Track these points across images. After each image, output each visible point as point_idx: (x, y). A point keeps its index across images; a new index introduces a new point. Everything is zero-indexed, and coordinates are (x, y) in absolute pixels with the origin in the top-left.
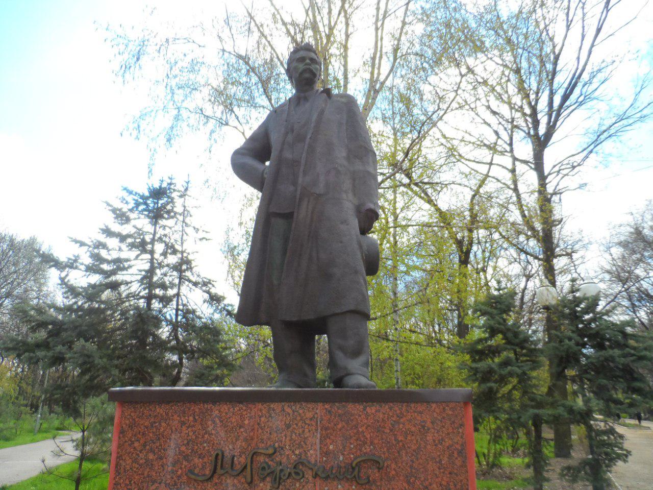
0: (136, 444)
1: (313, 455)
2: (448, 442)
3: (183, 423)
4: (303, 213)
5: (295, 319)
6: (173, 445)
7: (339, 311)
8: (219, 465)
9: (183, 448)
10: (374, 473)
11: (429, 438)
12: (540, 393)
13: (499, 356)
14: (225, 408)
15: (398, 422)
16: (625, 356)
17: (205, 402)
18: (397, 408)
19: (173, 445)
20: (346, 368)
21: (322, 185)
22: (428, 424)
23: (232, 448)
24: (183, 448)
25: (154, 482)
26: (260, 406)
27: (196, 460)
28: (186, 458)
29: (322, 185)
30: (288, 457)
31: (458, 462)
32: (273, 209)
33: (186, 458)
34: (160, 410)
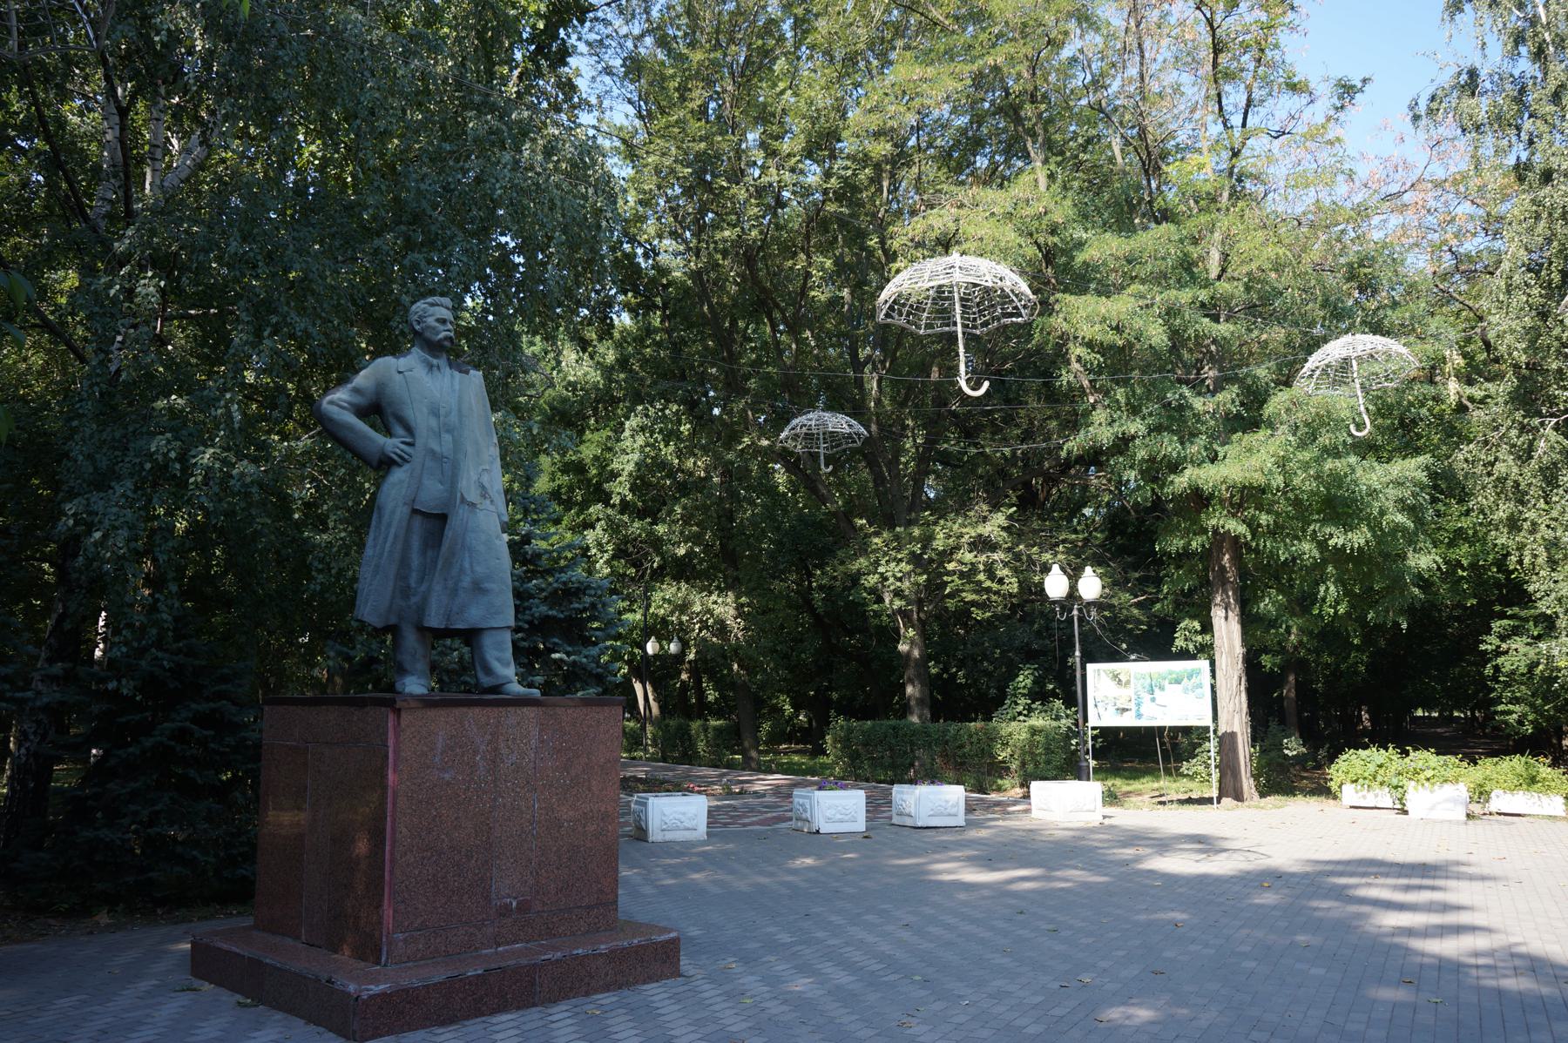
4: (454, 523)
14: (477, 710)
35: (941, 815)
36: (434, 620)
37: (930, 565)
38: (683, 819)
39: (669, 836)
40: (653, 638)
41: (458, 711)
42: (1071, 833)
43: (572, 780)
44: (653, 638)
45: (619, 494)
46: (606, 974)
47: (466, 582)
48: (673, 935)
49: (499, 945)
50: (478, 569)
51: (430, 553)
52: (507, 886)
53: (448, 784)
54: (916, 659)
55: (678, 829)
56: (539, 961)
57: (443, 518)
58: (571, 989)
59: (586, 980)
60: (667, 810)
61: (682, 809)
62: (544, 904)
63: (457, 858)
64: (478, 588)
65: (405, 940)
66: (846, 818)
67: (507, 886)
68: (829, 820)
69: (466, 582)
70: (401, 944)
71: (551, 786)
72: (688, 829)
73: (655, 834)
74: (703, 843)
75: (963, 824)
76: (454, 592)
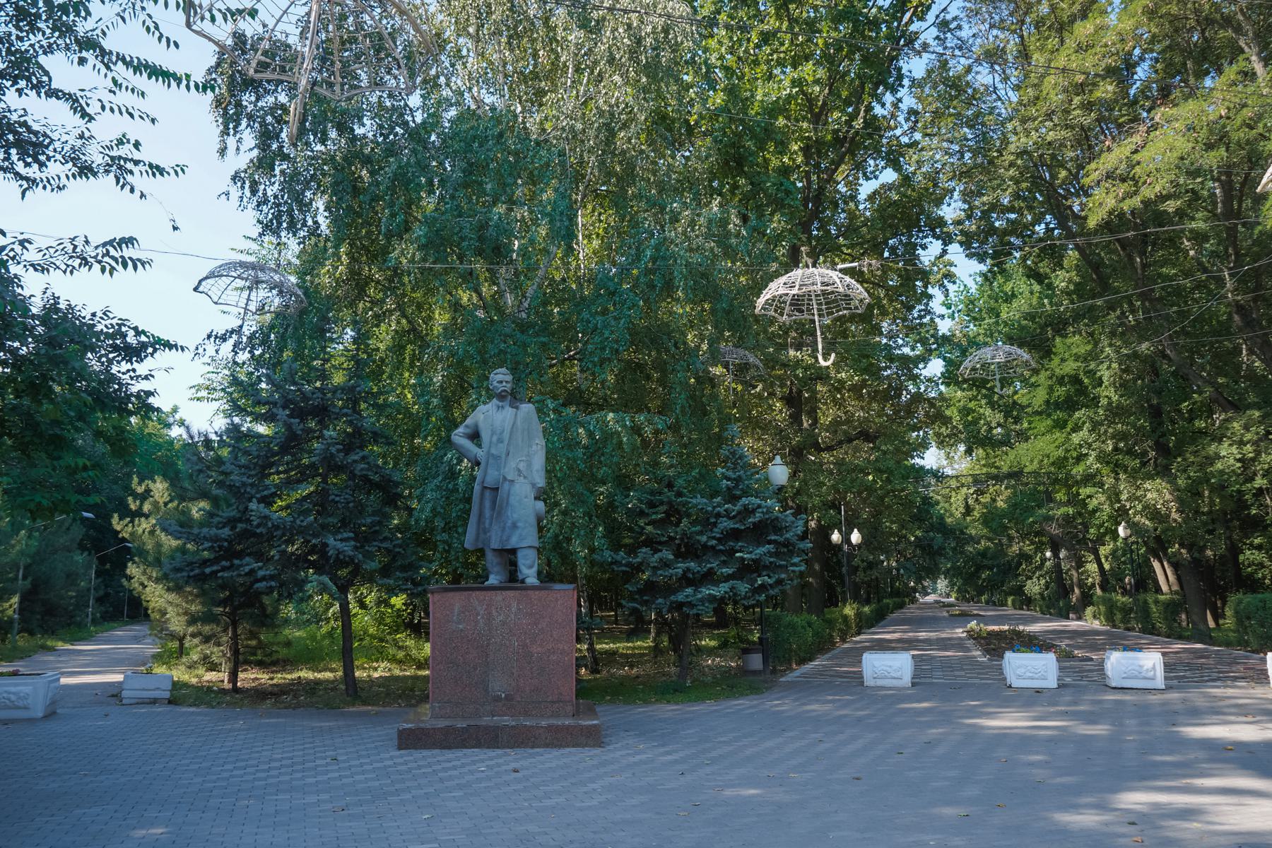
4: (503, 492)
35: (1136, 677)
38: (889, 670)
39: (880, 683)
40: (856, 530)
41: (466, 593)
44: (856, 530)
45: (1107, 397)
47: (509, 523)
49: (493, 716)
51: (970, 479)
52: (499, 685)
53: (462, 630)
54: (1249, 514)
55: (886, 678)
58: (522, 743)
60: (877, 664)
61: (889, 663)
66: (1036, 676)
67: (499, 685)
68: (1019, 677)
69: (509, 523)
72: (895, 678)
73: (869, 681)
74: (908, 688)
75: (1163, 687)
76: (503, 529)
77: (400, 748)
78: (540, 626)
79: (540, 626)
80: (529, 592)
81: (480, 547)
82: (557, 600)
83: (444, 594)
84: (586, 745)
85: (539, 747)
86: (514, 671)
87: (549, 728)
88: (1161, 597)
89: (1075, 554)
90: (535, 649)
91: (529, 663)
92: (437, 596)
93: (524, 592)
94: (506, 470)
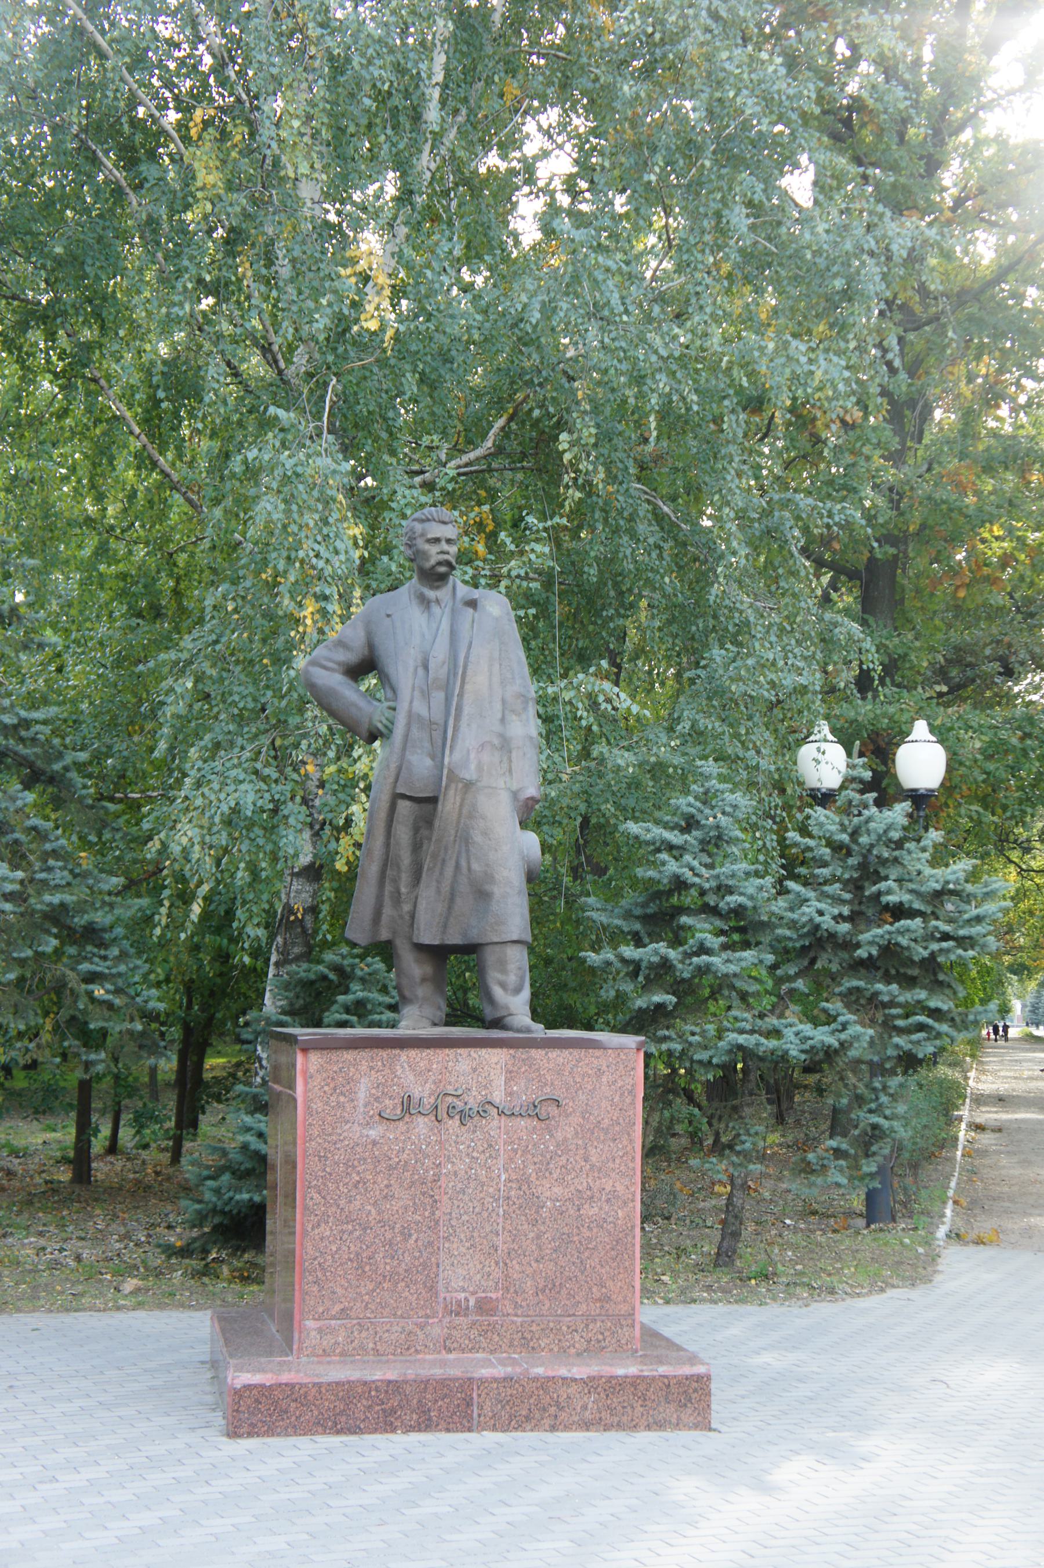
0: (326, 1088)
1: (498, 1096)
2: (620, 1083)
3: (372, 1068)
4: (449, 806)
5: (437, 943)
6: (363, 1089)
7: (496, 940)
8: (408, 1107)
9: (374, 1091)
10: (553, 1110)
11: (604, 1079)
12: (225, 1270)
13: (932, 45)
14: (413, 1053)
15: (576, 1066)
16: (930, 937)
17: (393, 1047)
18: (576, 1052)
19: (363, 1089)
20: (508, 1008)
21: (473, 767)
22: (604, 1068)
23: (422, 1091)
24: (374, 1091)
25: (347, 1122)
26: (447, 1051)
27: (387, 1102)
28: (377, 1099)
29: (473, 767)
30: (473, 1100)
31: (628, 1100)
32: (400, 790)
33: (377, 1099)
34: (349, 1055)
36: (428, 937)
37: (245, 462)
41: (384, 1053)
42: (216, 1325)
43: (558, 1145)
46: (585, 1407)
48: (701, 1369)
50: (475, 866)
53: (374, 1143)
56: (476, 1375)
57: (433, 800)
58: (528, 1419)
59: (553, 1410)
62: (516, 1306)
63: (388, 1236)
64: (482, 895)
65: (320, 1330)
70: (313, 1333)
71: (525, 1151)
77: (233, 1433)
78: (559, 1135)
79: (559, 1135)
80: (533, 1052)
81: (384, 935)
82: (599, 1073)
83: (334, 1055)
84: (677, 1426)
85: (567, 1428)
86: (499, 1241)
87: (590, 1384)
88: (176, 570)
89: (520, 508)
90: (550, 1191)
91: (534, 1223)
92: (315, 1059)
93: (521, 1053)
94: (457, 756)
